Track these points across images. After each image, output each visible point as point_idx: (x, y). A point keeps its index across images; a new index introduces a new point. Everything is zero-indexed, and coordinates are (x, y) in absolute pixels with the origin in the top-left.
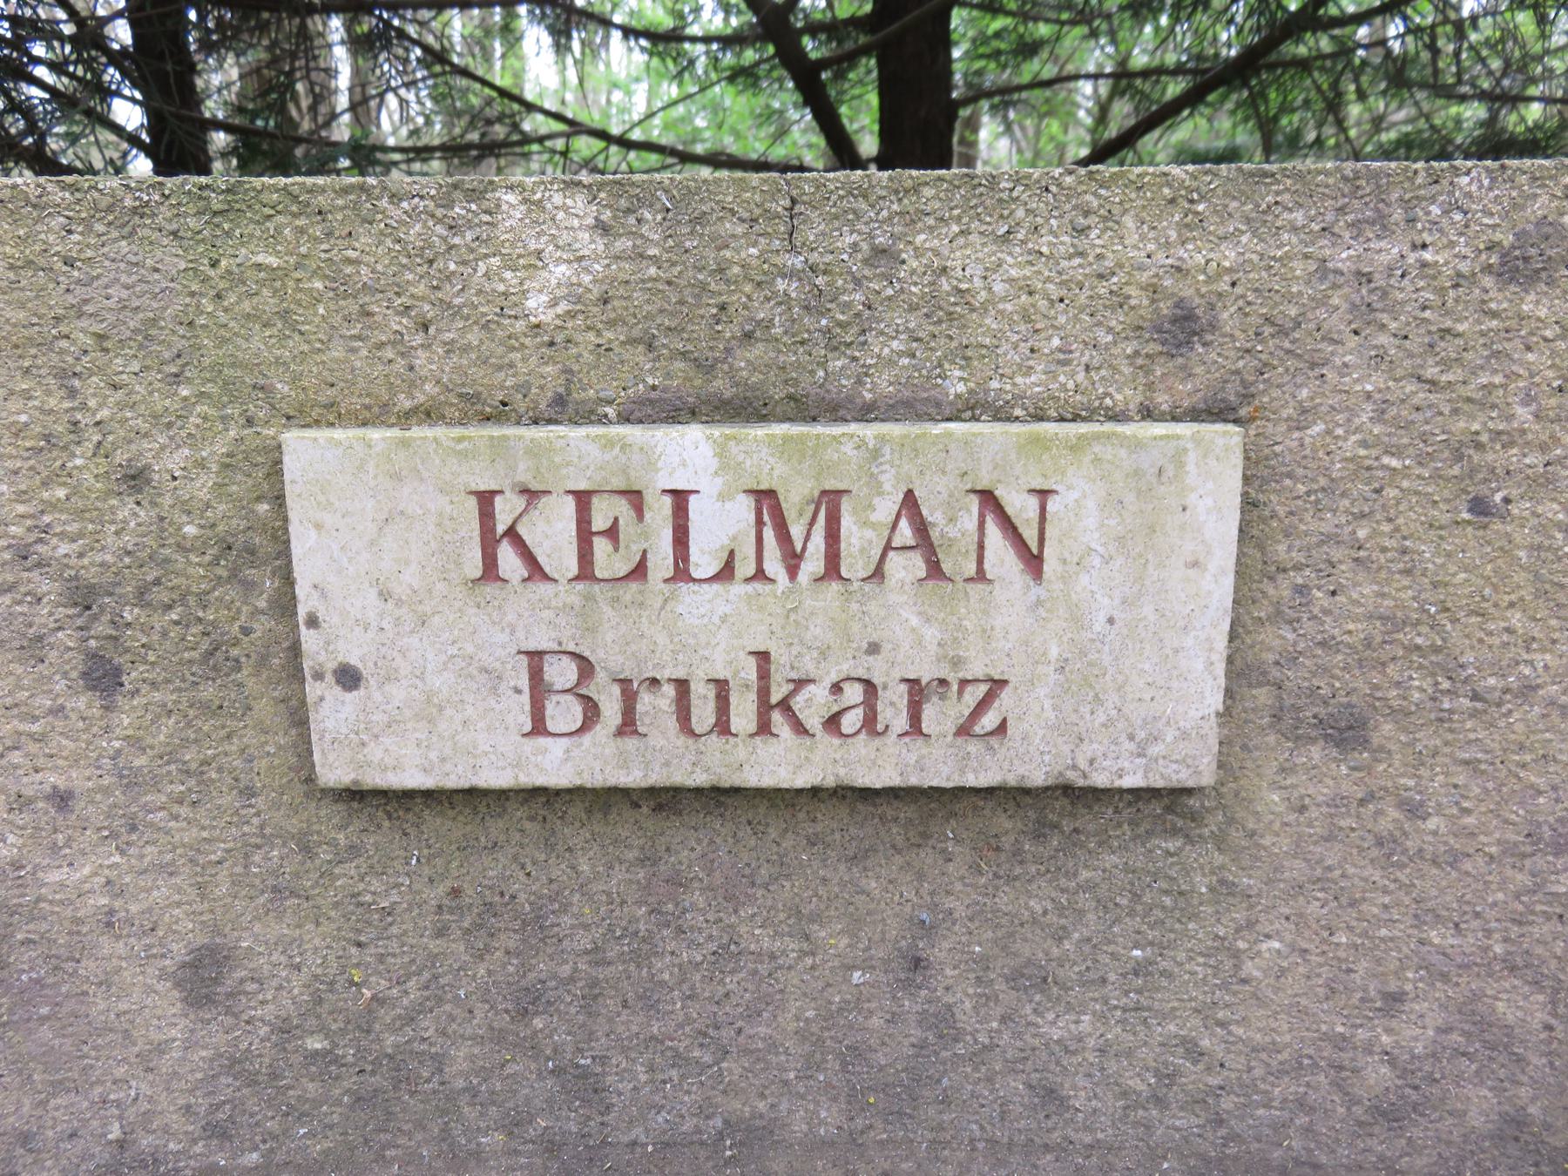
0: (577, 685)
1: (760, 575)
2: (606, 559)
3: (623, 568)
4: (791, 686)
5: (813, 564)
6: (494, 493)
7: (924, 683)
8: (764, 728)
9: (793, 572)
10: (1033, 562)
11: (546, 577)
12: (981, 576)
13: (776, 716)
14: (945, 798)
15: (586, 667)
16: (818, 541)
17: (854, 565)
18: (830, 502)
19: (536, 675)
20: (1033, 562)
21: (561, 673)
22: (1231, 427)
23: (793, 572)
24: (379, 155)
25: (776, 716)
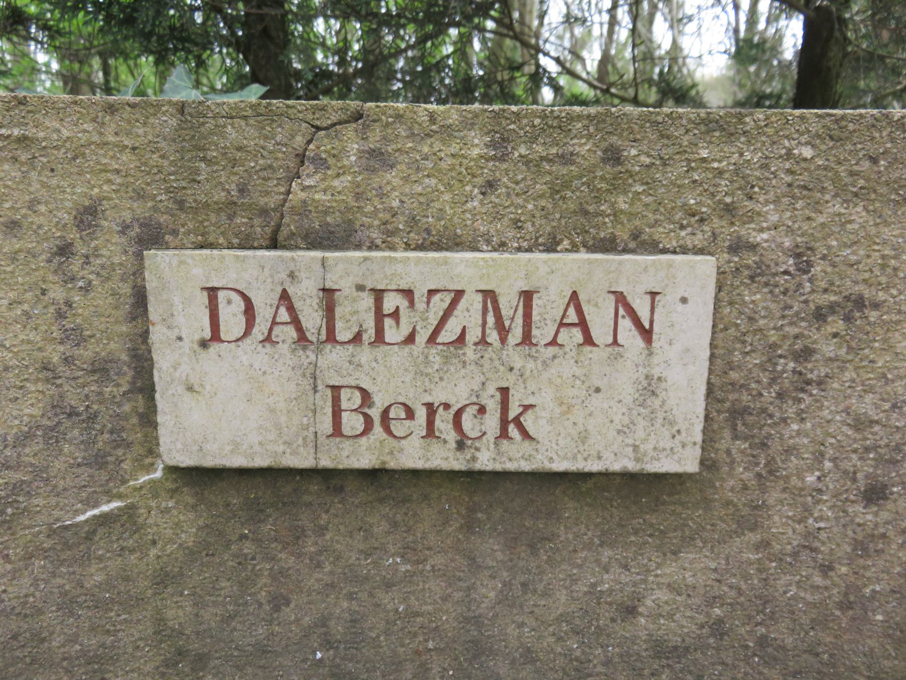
0: (360, 407)
1: (483, 342)
2: (392, 334)
3: (401, 338)
4: (521, 409)
5: (517, 333)
6: (383, 291)
7: (436, 405)
8: (504, 434)
9: (503, 340)
10: (647, 334)
11: (595, 345)
12: (615, 342)
13: (512, 428)
14: (590, 484)
15: (366, 395)
16: (519, 320)
17: (542, 333)
18: (527, 296)
19: (336, 401)
20: (647, 334)
21: (350, 400)
22: (709, 258)
23: (503, 340)
24: (742, 34)
25: (512, 428)
